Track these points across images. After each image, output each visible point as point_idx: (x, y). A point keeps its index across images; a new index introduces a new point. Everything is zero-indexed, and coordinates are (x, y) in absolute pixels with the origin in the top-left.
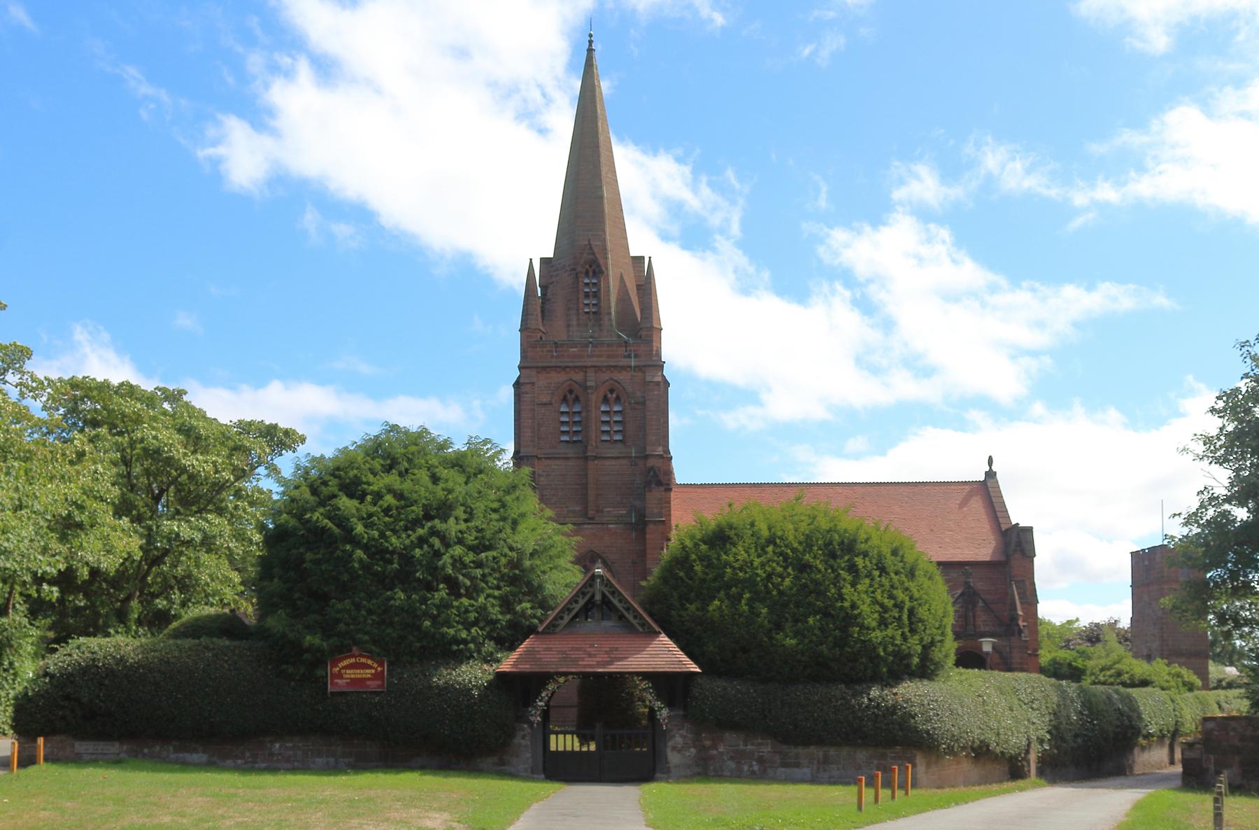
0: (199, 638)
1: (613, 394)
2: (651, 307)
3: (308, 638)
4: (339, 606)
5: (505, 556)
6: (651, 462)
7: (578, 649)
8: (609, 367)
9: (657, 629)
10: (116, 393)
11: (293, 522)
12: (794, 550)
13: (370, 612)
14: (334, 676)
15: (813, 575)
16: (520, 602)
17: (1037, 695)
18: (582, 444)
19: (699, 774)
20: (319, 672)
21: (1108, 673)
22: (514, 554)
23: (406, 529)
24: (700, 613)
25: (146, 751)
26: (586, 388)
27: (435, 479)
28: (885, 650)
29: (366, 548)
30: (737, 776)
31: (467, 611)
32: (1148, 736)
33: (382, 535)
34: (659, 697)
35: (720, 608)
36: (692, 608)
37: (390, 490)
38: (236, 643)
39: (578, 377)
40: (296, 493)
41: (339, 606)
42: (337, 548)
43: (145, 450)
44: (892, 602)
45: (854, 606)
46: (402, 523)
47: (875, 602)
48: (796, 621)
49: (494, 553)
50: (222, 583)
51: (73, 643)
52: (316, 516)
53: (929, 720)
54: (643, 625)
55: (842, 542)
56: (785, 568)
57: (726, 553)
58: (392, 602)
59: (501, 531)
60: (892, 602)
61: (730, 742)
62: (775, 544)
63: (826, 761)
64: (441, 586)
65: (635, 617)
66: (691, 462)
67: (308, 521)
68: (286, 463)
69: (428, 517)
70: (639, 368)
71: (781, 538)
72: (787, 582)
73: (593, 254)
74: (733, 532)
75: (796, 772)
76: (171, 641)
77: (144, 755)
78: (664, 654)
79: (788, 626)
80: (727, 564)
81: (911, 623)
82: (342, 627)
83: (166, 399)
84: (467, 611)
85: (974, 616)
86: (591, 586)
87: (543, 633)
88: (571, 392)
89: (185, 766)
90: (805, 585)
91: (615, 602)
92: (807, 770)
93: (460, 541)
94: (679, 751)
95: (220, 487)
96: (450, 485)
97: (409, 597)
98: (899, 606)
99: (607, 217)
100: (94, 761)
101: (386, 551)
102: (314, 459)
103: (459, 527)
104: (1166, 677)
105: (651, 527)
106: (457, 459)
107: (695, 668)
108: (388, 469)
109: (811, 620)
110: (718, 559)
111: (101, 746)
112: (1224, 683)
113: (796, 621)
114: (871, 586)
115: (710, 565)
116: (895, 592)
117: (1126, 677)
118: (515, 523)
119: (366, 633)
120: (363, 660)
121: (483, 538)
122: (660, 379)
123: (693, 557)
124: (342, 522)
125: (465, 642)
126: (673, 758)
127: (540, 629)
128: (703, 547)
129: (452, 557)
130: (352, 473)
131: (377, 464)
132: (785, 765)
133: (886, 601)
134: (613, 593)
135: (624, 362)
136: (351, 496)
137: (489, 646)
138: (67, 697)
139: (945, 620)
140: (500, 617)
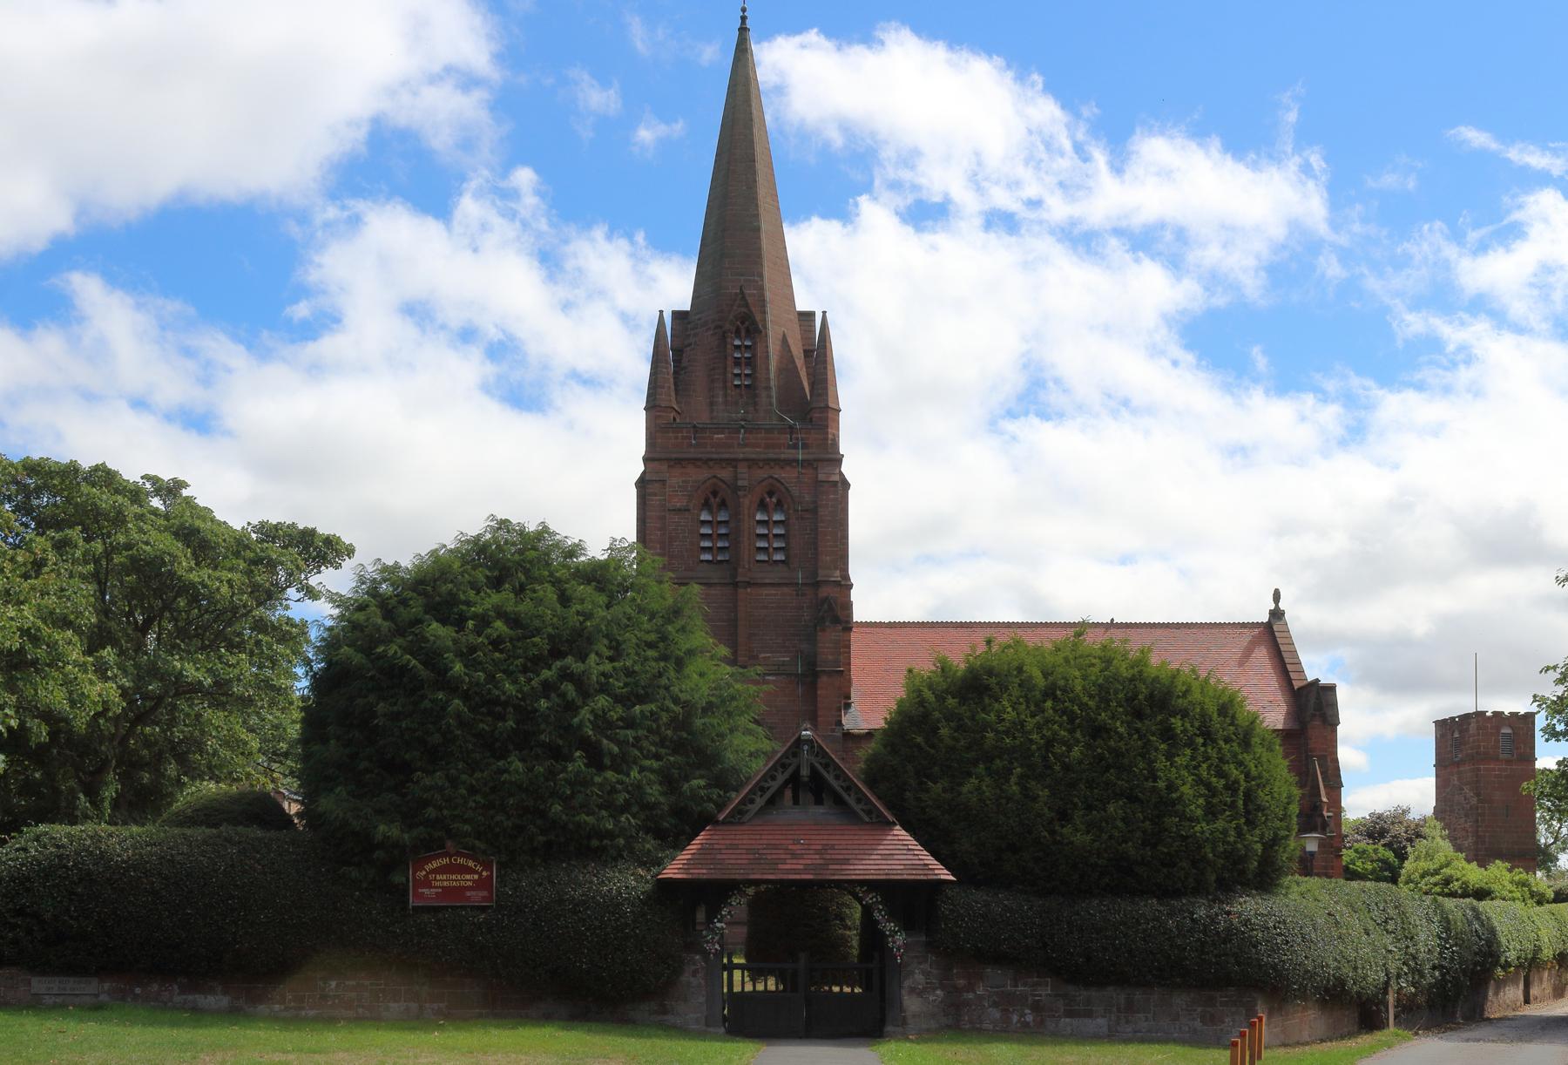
0: (216, 826)
1: (773, 497)
2: (825, 381)
3: (382, 828)
4: (427, 781)
5: (668, 710)
6: (824, 591)
7: (775, 847)
8: (767, 461)
9: (891, 818)
10: (85, 479)
11: (358, 658)
12: (1083, 706)
13: (473, 790)
14: (419, 884)
15: (1112, 743)
16: (687, 779)
17: (1391, 912)
18: (732, 565)
19: (949, 1027)
20: (397, 878)
21: (1433, 880)
22: (677, 709)
23: (525, 670)
24: (948, 796)
25: (138, 990)
26: (736, 489)
27: (565, 600)
28: (1213, 851)
29: (466, 697)
30: (1003, 1032)
31: (613, 791)
32: (1507, 965)
33: (491, 678)
34: (892, 916)
35: (978, 789)
36: (937, 788)
37: (501, 614)
38: (273, 834)
39: (725, 474)
40: (360, 616)
41: (427, 781)
42: (423, 697)
43: (133, 559)
44: (1223, 782)
45: (1171, 787)
46: (519, 662)
47: (1199, 781)
48: (1089, 808)
49: (653, 707)
50: (255, 751)
51: (30, 831)
52: (393, 649)
53: (1275, 949)
54: (869, 813)
55: (1151, 695)
56: (1072, 731)
57: (983, 710)
58: (505, 776)
59: (660, 675)
60: (1223, 782)
61: (994, 980)
62: (1055, 699)
64: (578, 754)
65: (859, 801)
66: (874, 597)
67: (382, 656)
68: (338, 580)
69: (556, 654)
70: (807, 463)
71: (1064, 691)
72: (1076, 752)
73: (747, 305)
74: (993, 680)
75: (1091, 1025)
76: (177, 831)
77: (136, 997)
78: (900, 854)
79: (1078, 816)
80: (986, 726)
81: (1248, 812)
82: (431, 812)
83: (157, 492)
84: (613, 791)
86: (795, 755)
87: (724, 823)
88: (715, 494)
89: (198, 1015)
90: (1101, 758)
91: (830, 778)
92: (1101, 1021)
93: (604, 689)
94: (920, 994)
95: (233, 613)
96: (588, 606)
97: (530, 770)
98: (1232, 787)
100: (59, 1007)
101: (496, 701)
102: (385, 569)
103: (601, 668)
104: (1509, 886)
105: (824, 679)
106: (594, 570)
107: (945, 875)
108: (496, 584)
109: (1111, 808)
110: (973, 718)
111: (71, 984)
112: (1456, 885)
113: (1089, 808)
114: (1193, 758)
115: (960, 728)
116: (1226, 767)
117: (1456, 885)
118: (680, 664)
119: (465, 821)
120: (461, 861)
121: (636, 684)
122: (836, 478)
123: (937, 714)
124: (432, 658)
125: (610, 835)
126: (912, 1004)
127: (721, 817)
128: (951, 702)
129: (592, 711)
130: (445, 588)
131: (480, 575)
132: (1070, 1014)
133: (1214, 780)
134: (826, 766)
135: (787, 454)
136: (444, 622)
137: (650, 844)
138: (20, 912)
139: (1291, 807)
140: (662, 799)
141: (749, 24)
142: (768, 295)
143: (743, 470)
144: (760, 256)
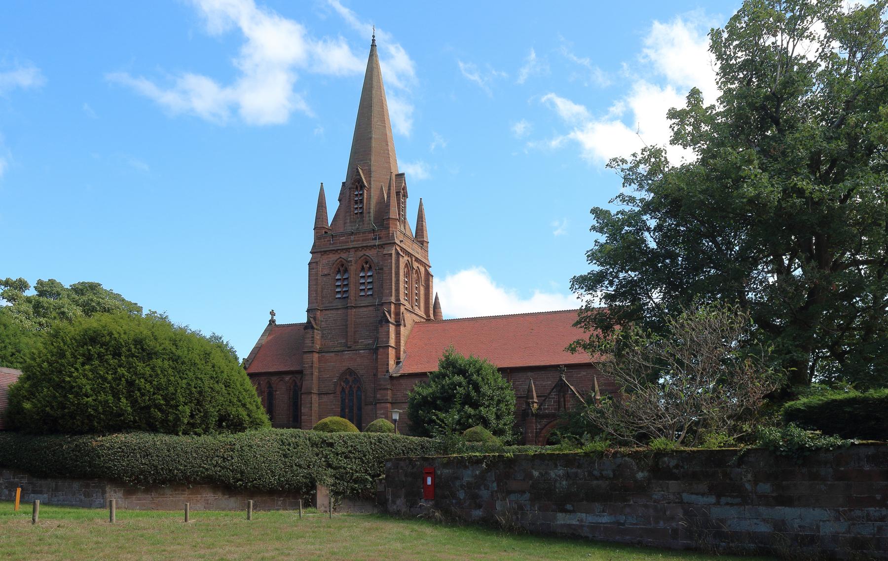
1: (367, 264)
39: (344, 256)
63: (56, 489)
70: (381, 246)
85: (564, 401)
99: (373, 150)
135: (372, 243)
141: (376, 43)
142: (373, 169)
143: (352, 252)
144: (370, 150)
